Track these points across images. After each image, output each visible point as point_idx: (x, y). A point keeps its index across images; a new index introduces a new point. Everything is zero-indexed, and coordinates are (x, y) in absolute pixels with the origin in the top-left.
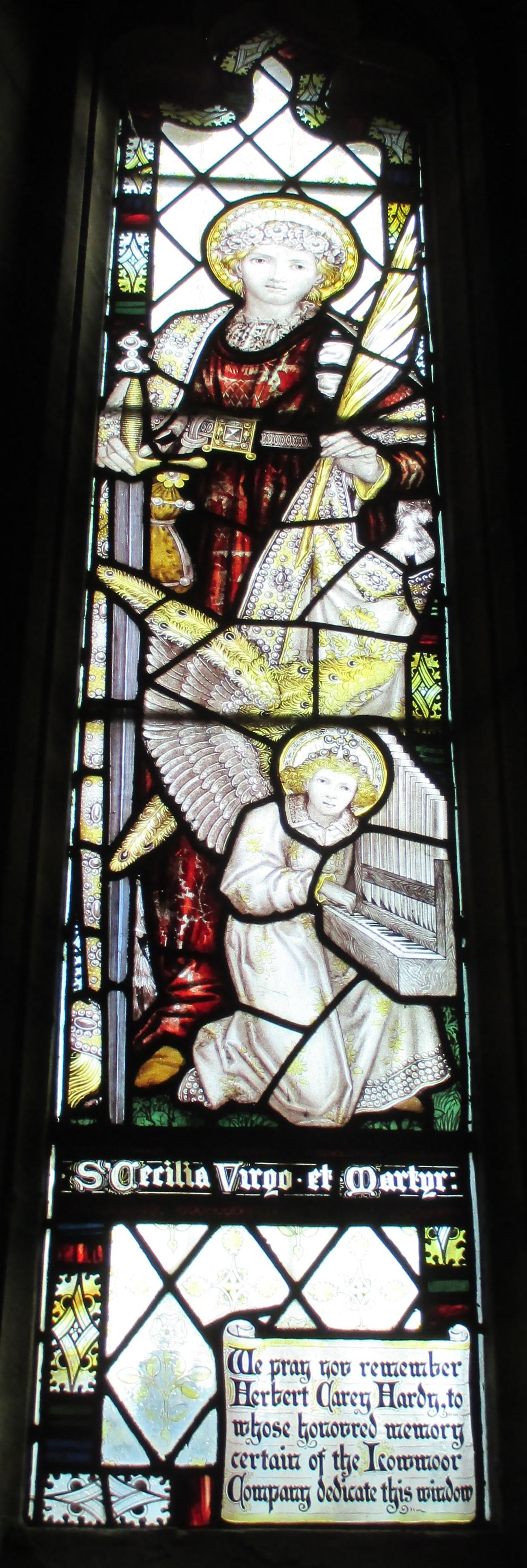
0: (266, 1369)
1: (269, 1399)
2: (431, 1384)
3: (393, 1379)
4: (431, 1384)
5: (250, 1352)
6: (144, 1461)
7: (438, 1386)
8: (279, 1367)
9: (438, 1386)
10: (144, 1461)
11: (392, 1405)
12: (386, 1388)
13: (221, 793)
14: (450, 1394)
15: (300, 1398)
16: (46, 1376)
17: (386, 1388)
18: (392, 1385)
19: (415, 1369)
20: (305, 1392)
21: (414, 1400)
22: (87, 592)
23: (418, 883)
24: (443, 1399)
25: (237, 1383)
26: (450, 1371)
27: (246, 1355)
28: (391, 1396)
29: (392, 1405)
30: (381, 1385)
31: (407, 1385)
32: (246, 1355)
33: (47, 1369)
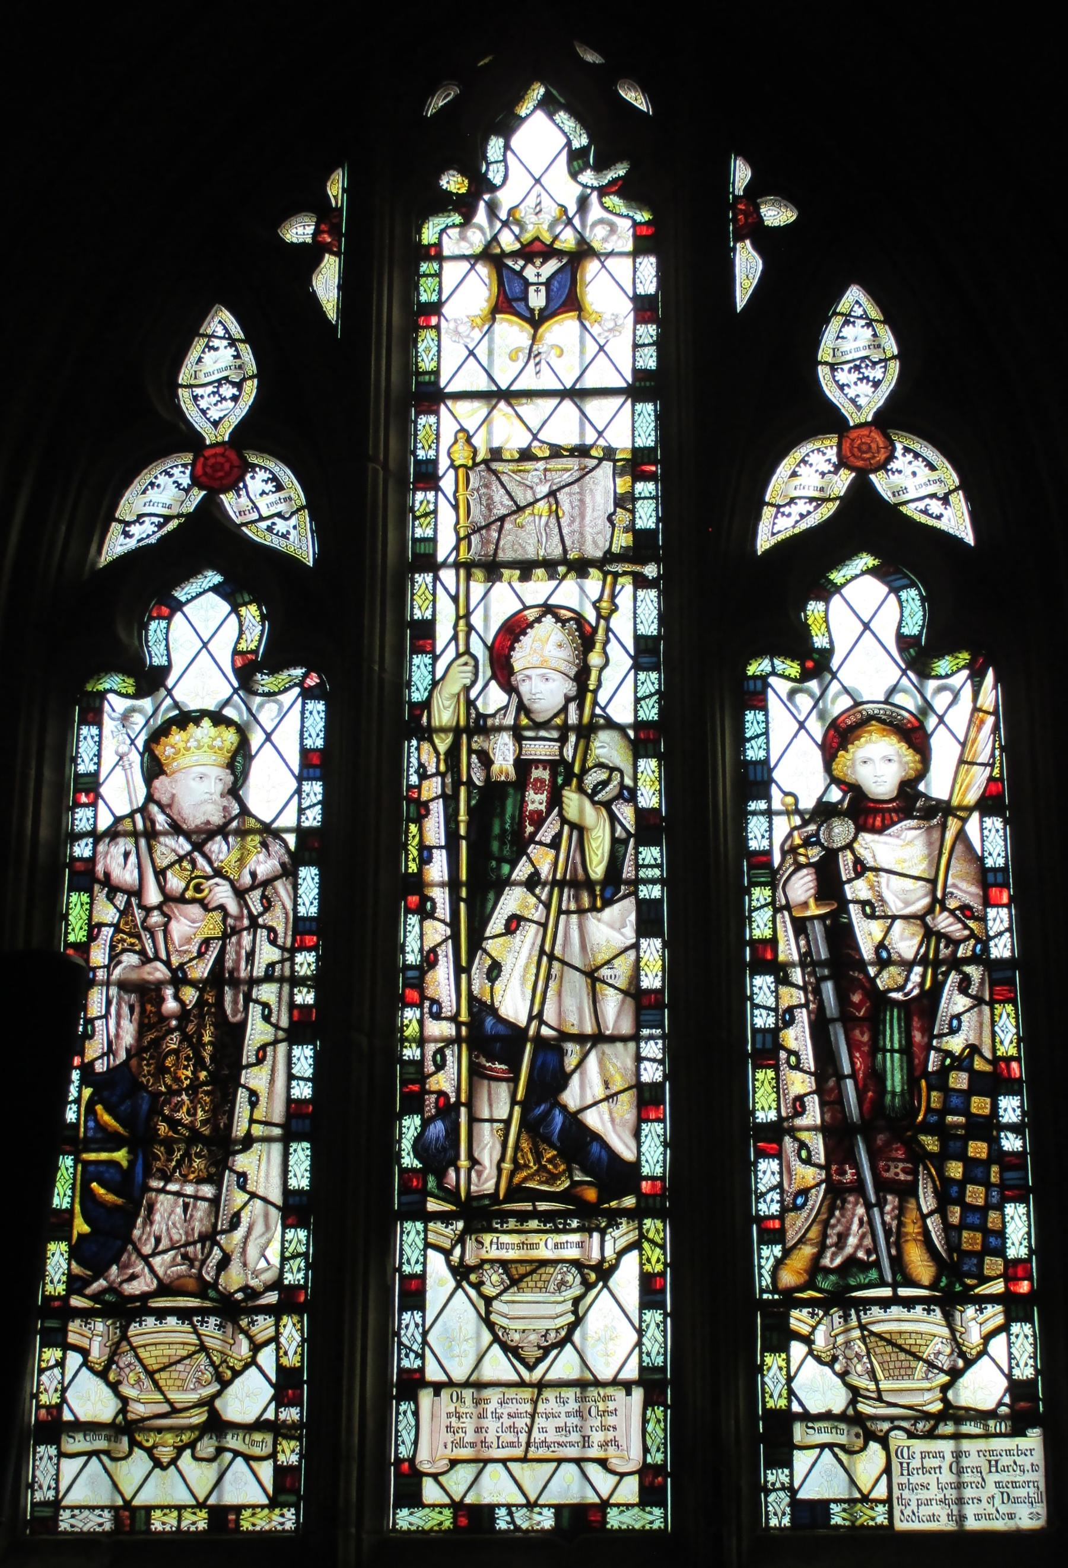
0: (918, 1456)
1: (920, 1471)
2: (1020, 1460)
3: (996, 1458)
4: (1020, 1460)
5: (908, 1448)
6: (194, 1503)
7: (1025, 1461)
8: (924, 1455)
9: (1025, 1461)
10: (194, 1503)
11: (997, 1471)
12: (993, 1463)
13: (595, 630)
14: (1032, 1465)
15: (937, 1471)
16: (396, 1449)
17: (993, 1463)
18: (997, 1461)
19: (1009, 1452)
20: (940, 1467)
21: (1010, 1469)
22: (482, 63)
23: (880, 831)
24: (1028, 1467)
25: (901, 1464)
26: (1028, 1453)
27: (905, 1449)
28: (997, 1467)
29: (997, 1471)
30: (990, 1462)
31: (1005, 1461)
32: (905, 1449)
33: (397, 1446)
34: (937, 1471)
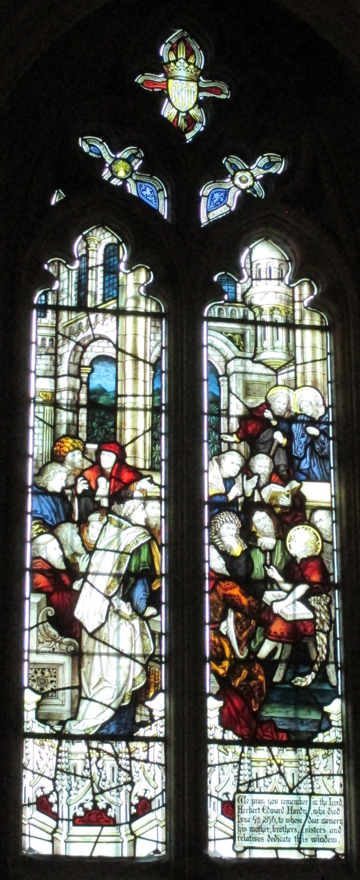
1: (248, 811)
5: (245, 797)
15: (257, 811)
20: (259, 809)
34: (257, 811)
